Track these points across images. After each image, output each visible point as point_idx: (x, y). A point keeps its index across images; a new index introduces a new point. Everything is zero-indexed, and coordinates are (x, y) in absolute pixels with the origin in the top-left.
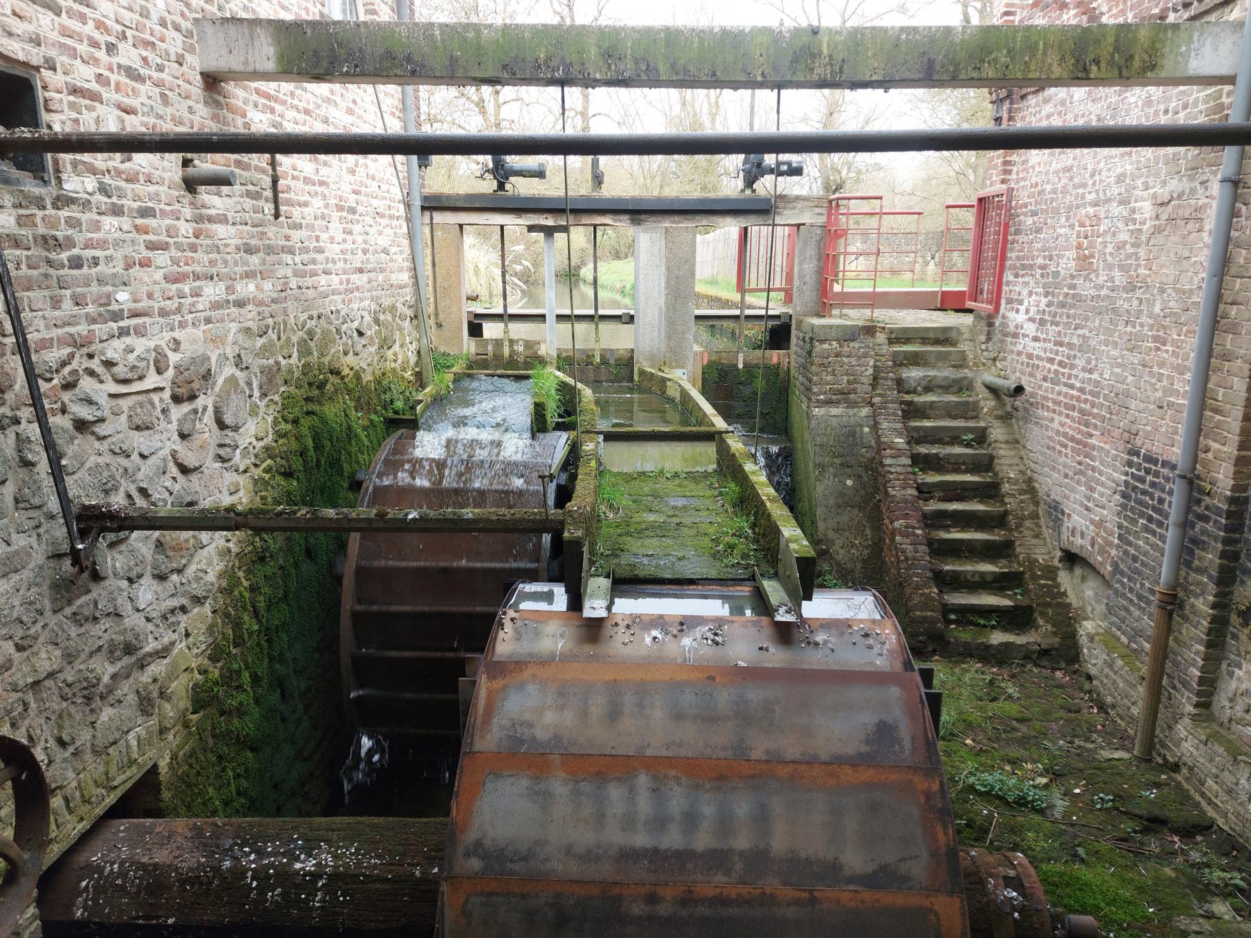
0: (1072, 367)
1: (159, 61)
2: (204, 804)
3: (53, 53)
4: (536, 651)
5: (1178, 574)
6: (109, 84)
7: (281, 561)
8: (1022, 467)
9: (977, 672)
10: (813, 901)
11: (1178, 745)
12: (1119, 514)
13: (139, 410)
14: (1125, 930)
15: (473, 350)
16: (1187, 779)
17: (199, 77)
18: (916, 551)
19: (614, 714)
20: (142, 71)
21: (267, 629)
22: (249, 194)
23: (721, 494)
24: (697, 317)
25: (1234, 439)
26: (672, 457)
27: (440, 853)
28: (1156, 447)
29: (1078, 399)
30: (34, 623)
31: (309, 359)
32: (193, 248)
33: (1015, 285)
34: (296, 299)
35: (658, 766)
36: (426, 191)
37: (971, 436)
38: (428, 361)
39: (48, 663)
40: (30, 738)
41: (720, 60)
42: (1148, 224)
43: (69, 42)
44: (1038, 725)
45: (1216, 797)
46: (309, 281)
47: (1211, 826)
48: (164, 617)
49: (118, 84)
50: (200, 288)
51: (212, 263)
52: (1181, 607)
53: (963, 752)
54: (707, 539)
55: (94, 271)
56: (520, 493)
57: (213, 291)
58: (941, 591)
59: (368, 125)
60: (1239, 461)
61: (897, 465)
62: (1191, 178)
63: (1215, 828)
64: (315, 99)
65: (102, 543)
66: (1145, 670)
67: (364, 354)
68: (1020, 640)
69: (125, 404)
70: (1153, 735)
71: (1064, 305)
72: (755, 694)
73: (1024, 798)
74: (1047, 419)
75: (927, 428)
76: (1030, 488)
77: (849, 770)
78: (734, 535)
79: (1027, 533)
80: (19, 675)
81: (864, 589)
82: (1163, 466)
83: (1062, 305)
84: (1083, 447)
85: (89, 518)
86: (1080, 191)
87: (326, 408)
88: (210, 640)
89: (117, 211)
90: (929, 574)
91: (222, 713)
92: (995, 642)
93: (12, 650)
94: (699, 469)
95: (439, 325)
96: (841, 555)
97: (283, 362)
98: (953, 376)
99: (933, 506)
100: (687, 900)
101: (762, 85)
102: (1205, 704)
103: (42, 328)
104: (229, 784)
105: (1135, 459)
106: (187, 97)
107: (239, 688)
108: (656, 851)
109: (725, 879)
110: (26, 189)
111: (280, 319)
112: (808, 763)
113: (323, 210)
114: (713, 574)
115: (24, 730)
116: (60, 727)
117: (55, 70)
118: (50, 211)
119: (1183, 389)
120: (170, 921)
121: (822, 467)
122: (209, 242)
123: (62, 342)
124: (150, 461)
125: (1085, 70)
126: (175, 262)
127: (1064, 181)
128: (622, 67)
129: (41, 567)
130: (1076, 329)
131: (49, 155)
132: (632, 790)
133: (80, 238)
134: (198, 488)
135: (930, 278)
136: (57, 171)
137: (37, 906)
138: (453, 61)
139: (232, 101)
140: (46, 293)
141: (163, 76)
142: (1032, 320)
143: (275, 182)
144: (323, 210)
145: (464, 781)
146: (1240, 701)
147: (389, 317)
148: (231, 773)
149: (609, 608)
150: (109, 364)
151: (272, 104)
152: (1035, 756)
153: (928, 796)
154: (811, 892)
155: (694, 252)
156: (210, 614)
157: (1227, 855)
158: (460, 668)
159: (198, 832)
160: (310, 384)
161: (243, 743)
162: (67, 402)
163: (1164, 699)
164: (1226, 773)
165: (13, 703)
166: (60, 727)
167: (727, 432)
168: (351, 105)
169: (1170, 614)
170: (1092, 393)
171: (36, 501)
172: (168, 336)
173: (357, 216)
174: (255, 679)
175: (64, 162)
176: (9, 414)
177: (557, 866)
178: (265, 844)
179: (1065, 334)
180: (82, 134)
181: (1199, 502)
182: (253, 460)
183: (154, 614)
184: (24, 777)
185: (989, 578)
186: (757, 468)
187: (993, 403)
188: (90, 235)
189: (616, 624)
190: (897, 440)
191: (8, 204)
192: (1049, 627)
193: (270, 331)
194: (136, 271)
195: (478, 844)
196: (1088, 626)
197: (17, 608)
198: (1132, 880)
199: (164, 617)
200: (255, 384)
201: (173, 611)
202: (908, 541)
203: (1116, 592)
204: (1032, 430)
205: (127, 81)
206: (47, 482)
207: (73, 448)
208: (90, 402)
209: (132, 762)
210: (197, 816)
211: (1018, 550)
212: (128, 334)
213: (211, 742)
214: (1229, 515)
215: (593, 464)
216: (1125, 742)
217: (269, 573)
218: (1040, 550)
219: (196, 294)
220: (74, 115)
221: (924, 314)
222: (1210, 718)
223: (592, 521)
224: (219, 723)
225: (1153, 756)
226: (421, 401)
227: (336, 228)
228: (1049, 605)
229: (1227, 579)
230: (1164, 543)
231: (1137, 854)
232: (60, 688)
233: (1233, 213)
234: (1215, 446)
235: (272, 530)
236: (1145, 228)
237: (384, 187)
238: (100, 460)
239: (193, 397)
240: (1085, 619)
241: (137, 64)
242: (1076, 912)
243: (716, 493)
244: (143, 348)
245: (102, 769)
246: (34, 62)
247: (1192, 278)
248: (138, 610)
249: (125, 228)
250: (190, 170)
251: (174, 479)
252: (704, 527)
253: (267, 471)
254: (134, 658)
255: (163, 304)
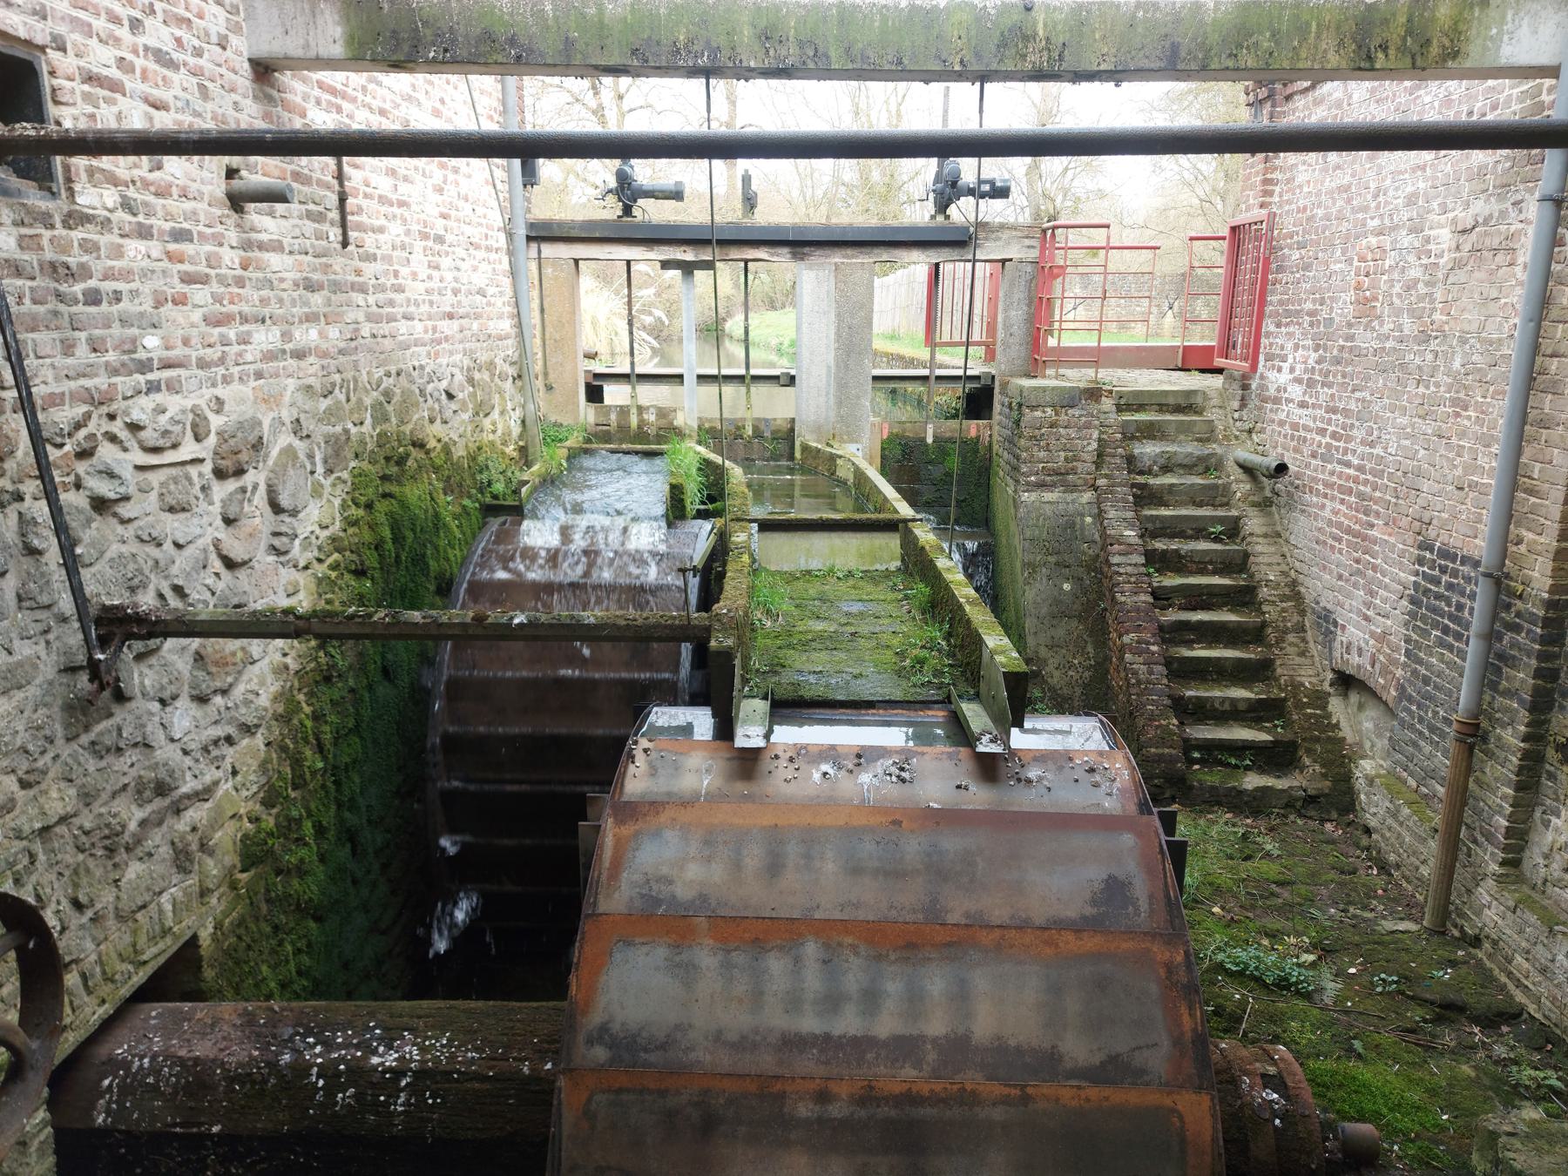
0: (1349, 439)
1: (196, 43)
2: (256, 985)
3: (62, 29)
4: (675, 789)
5: (1481, 699)
6: (133, 71)
7: (351, 682)
8: (1286, 568)
9: (1226, 823)
10: (1026, 1099)
11: (1479, 914)
12: (1406, 624)
13: (172, 487)
14: (1412, 1141)
15: (591, 419)
16: (1490, 956)
17: (246, 65)
18: (1151, 673)
19: (774, 867)
20: (175, 56)
21: (335, 767)
22: (309, 215)
23: (906, 597)
24: (875, 378)
25: (1553, 528)
26: (846, 551)
27: (555, 1045)
28: (1455, 541)
29: (1356, 481)
30: (43, 753)
31: (385, 426)
32: (240, 282)
33: (1276, 337)
34: (370, 350)
35: (830, 931)
36: (531, 217)
37: (1220, 528)
38: (536, 432)
39: (61, 804)
40: (38, 897)
41: (907, 43)
42: (1446, 258)
43: (82, 15)
44: (1303, 889)
45: (1527, 978)
46: (385, 328)
47: (1520, 1014)
48: (206, 750)
49: (144, 71)
50: (249, 333)
51: (264, 302)
52: (1485, 740)
53: (1209, 923)
54: (889, 652)
55: (115, 308)
56: (655, 590)
57: (265, 338)
58: (1182, 723)
59: (462, 122)
60: (1559, 555)
61: (1128, 563)
62: (1501, 198)
63: (1525, 1016)
64: (393, 96)
65: (127, 655)
66: (1438, 820)
67: (455, 422)
68: (1281, 784)
69: (155, 478)
70: (1448, 902)
71: (1338, 361)
72: (952, 843)
73: (1286, 979)
74: (1315, 505)
75: (1165, 517)
76: (1294, 593)
77: (1070, 937)
78: (923, 647)
79: (1290, 650)
80: (24, 819)
81: (1087, 714)
82: (1462, 564)
83: (1337, 361)
84: (1362, 541)
85: (111, 621)
86: (1360, 216)
87: (407, 490)
88: (263, 780)
89: (144, 233)
90: (1167, 702)
91: (278, 872)
92: (1250, 787)
93: (15, 787)
94: (878, 567)
95: (549, 388)
96: (1056, 678)
97: (354, 430)
98: (1197, 453)
99: (1173, 616)
100: (867, 1097)
101: (959, 77)
102: (1513, 862)
103: (50, 379)
104: (287, 961)
105: (1428, 555)
106: (232, 90)
107: (300, 841)
108: (827, 1037)
109: (914, 1073)
110: (30, 203)
111: (349, 375)
112: (1020, 928)
113: (403, 237)
114: (898, 695)
115: (30, 888)
116: (76, 886)
117: (64, 50)
118: (60, 231)
119: (1489, 466)
120: (215, 1129)
121: (1032, 567)
122: (260, 275)
123: (75, 398)
124: (188, 552)
125: (1369, 58)
126: (218, 299)
127: (1340, 203)
128: (784, 52)
129: (51, 683)
130: (1353, 391)
131: (58, 159)
132: (797, 960)
133: (98, 266)
134: (247, 588)
135: (1168, 334)
136: (69, 180)
137: (49, 1109)
138: (569, 43)
139: (288, 96)
140: (55, 335)
141: (201, 62)
142: (1298, 381)
143: (342, 200)
144: (403, 237)
145: (584, 950)
146: (1558, 857)
147: (486, 376)
148: (289, 948)
149: (767, 736)
150: (134, 427)
151: (339, 101)
152: (1300, 928)
153: (1170, 968)
154: (1023, 1087)
155: (872, 294)
156: (262, 747)
157: (1539, 1049)
158: (578, 809)
159: (250, 1019)
160: (387, 459)
161: (304, 910)
162: (82, 474)
163: (1462, 856)
164: (1540, 947)
165: (16, 854)
166: (76, 886)
167: (914, 520)
168: (438, 105)
169: (1471, 748)
170: (1373, 472)
171: (44, 599)
172: (208, 393)
173: (445, 247)
174: (320, 831)
175: (77, 170)
176: (10, 487)
177: (703, 1056)
178: (334, 1034)
179: (1340, 399)
180: (100, 131)
181: (1508, 607)
182: (316, 553)
183: (193, 746)
184: (31, 945)
185: (1242, 706)
186: (951, 564)
187: (1248, 487)
188: (110, 263)
189: (777, 757)
190: (1127, 533)
191: (7, 220)
192: (1317, 767)
193: (337, 391)
194: (168, 310)
195: (604, 1028)
196: (1367, 766)
197: (21, 734)
198: (1422, 1080)
199: (206, 750)
200: (318, 458)
201: (216, 742)
202: (1141, 660)
203: (1402, 723)
204: (1297, 521)
205: (157, 67)
206: (59, 576)
207: (92, 534)
208: (111, 475)
209: (166, 932)
210: (247, 1000)
211: (1279, 671)
212: (159, 389)
213: (264, 908)
214: (1546, 622)
215: (746, 558)
216: (1411, 909)
217: (336, 696)
218: (1305, 670)
219: (244, 340)
220: (90, 109)
221: (1161, 375)
222: (1520, 879)
223: (744, 628)
224: (275, 884)
225: (1447, 924)
226: (526, 483)
227: (419, 262)
228: (1317, 740)
229: (1541, 705)
230: (1464, 660)
231: (1427, 1048)
232: (75, 837)
233: (1556, 241)
234: (1529, 536)
235: (342, 637)
236: (1442, 261)
237: (480, 210)
238: (124, 549)
239: (240, 472)
240: (1362, 757)
241: (168, 46)
242: (1352, 1119)
243: (901, 596)
244: (177, 408)
245: (128, 939)
246: (39, 40)
247: (1501, 324)
248: (172, 740)
249: (155, 254)
250: (236, 183)
251: (217, 575)
252: (886, 638)
253: (334, 567)
254: (167, 801)
255: (202, 352)
